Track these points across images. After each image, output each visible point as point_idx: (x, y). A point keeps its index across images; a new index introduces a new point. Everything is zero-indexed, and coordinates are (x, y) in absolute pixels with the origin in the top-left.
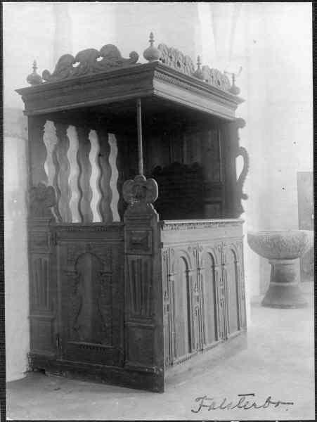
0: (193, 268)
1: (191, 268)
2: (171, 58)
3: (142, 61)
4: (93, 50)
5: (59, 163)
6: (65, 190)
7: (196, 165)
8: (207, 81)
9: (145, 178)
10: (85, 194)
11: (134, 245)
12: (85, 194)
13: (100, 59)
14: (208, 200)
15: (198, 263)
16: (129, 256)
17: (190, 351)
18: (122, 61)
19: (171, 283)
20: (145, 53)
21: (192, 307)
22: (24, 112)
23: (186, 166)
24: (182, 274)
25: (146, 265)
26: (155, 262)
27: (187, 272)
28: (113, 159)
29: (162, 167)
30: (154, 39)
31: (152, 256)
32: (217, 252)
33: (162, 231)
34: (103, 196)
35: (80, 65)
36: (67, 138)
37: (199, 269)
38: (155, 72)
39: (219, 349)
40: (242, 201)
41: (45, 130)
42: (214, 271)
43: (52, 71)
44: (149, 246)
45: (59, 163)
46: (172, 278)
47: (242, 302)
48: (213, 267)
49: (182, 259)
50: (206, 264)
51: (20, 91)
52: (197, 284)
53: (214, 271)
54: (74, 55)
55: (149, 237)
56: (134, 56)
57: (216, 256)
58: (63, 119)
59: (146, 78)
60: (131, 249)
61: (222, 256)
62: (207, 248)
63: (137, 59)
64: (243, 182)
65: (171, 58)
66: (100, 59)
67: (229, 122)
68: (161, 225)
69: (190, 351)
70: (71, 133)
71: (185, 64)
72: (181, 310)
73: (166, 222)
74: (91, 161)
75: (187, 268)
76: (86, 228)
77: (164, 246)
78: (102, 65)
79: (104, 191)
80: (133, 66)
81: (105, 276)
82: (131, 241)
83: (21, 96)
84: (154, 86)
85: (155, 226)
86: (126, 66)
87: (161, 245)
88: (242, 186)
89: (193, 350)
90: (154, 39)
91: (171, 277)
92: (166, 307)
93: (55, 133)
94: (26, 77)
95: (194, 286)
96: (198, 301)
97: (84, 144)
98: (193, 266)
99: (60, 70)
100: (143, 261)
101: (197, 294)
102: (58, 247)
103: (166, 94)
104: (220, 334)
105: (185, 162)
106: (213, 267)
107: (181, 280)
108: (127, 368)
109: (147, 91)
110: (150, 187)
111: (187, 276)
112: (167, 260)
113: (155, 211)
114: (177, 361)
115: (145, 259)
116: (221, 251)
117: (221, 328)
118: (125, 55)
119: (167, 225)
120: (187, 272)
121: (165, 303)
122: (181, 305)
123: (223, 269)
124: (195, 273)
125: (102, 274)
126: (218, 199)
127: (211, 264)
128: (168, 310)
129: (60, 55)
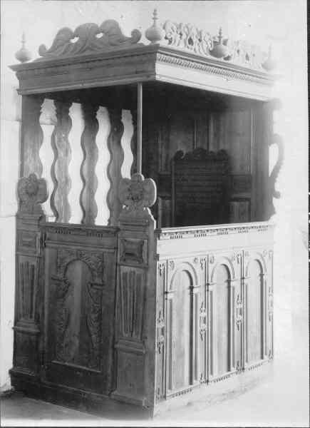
0: (200, 282)
1: (197, 283)
2: (181, 34)
3: (145, 41)
4: (94, 26)
5: (58, 146)
6: (63, 180)
7: (223, 152)
8: (228, 58)
9: (143, 177)
10: (89, 183)
11: (129, 254)
12: (89, 183)
13: (100, 36)
14: (235, 196)
15: (206, 276)
16: (122, 267)
17: (191, 383)
18: (122, 40)
19: (168, 301)
20: (146, 33)
21: (233, 320)
22: (18, 90)
23: (211, 152)
24: (184, 292)
25: (139, 280)
26: (149, 275)
27: (191, 288)
28: (126, 142)
29: (185, 152)
30: (157, 16)
31: (146, 269)
32: (235, 262)
33: (158, 241)
34: (111, 182)
35: (78, 41)
36: (69, 120)
37: (208, 284)
38: (158, 54)
39: (234, 381)
40: (274, 199)
41: (42, 110)
42: (229, 287)
43: (49, 46)
44: (142, 255)
45: (58, 146)
46: (170, 296)
47: (269, 324)
48: (229, 281)
49: (186, 274)
50: (218, 277)
51: (13, 68)
52: (205, 304)
53: (229, 287)
54: (73, 30)
55: (145, 245)
56: (137, 36)
57: (233, 269)
58: (63, 100)
59: (153, 53)
60: (125, 260)
61: (242, 269)
62: (220, 259)
63: (139, 39)
64: (276, 177)
65: (181, 34)
66: (100, 36)
67: (263, 102)
68: (158, 233)
69: (191, 383)
70: (76, 112)
71: (200, 40)
72: (180, 332)
73: (164, 230)
74: (98, 145)
75: (192, 283)
76: (87, 228)
77: (160, 259)
78: (102, 43)
79: (112, 178)
80: (134, 46)
81: (95, 289)
82: (125, 249)
83: (15, 72)
84: (156, 71)
85: (152, 235)
86: (126, 47)
87: (157, 257)
88: (274, 181)
89: (194, 381)
90: (157, 16)
91: (168, 295)
92: (160, 331)
93: (55, 112)
94: (14, 52)
95: (199, 306)
96: (205, 322)
97: (91, 124)
98: (199, 282)
99: (58, 44)
100: (137, 273)
101: (204, 314)
102: (47, 250)
103: (172, 78)
104: (235, 362)
105: (211, 148)
106: (229, 281)
107: (183, 300)
108: (113, 397)
109: (148, 76)
110: (147, 188)
111: (191, 294)
112: (164, 275)
113: (152, 217)
114: (249, 367)
115: (138, 271)
116: (241, 262)
117: (236, 357)
118: (127, 33)
119: (165, 234)
120: (191, 288)
121: (159, 326)
122: (181, 326)
123: (242, 284)
124: (203, 290)
125: (92, 285)
126: (244, 195)
127: (226, 278)
128: (163, 334)
129: (63, 27)
